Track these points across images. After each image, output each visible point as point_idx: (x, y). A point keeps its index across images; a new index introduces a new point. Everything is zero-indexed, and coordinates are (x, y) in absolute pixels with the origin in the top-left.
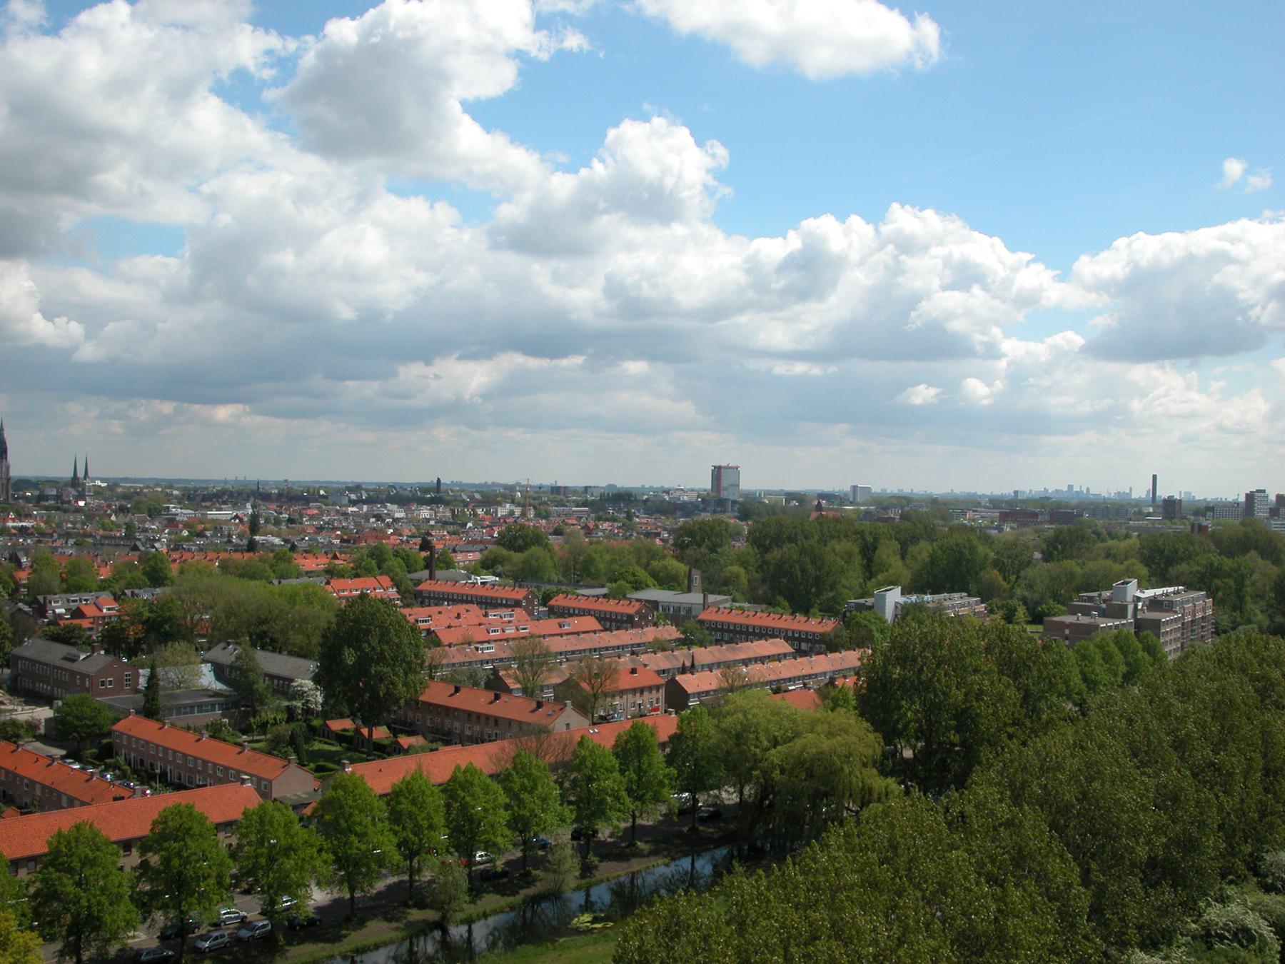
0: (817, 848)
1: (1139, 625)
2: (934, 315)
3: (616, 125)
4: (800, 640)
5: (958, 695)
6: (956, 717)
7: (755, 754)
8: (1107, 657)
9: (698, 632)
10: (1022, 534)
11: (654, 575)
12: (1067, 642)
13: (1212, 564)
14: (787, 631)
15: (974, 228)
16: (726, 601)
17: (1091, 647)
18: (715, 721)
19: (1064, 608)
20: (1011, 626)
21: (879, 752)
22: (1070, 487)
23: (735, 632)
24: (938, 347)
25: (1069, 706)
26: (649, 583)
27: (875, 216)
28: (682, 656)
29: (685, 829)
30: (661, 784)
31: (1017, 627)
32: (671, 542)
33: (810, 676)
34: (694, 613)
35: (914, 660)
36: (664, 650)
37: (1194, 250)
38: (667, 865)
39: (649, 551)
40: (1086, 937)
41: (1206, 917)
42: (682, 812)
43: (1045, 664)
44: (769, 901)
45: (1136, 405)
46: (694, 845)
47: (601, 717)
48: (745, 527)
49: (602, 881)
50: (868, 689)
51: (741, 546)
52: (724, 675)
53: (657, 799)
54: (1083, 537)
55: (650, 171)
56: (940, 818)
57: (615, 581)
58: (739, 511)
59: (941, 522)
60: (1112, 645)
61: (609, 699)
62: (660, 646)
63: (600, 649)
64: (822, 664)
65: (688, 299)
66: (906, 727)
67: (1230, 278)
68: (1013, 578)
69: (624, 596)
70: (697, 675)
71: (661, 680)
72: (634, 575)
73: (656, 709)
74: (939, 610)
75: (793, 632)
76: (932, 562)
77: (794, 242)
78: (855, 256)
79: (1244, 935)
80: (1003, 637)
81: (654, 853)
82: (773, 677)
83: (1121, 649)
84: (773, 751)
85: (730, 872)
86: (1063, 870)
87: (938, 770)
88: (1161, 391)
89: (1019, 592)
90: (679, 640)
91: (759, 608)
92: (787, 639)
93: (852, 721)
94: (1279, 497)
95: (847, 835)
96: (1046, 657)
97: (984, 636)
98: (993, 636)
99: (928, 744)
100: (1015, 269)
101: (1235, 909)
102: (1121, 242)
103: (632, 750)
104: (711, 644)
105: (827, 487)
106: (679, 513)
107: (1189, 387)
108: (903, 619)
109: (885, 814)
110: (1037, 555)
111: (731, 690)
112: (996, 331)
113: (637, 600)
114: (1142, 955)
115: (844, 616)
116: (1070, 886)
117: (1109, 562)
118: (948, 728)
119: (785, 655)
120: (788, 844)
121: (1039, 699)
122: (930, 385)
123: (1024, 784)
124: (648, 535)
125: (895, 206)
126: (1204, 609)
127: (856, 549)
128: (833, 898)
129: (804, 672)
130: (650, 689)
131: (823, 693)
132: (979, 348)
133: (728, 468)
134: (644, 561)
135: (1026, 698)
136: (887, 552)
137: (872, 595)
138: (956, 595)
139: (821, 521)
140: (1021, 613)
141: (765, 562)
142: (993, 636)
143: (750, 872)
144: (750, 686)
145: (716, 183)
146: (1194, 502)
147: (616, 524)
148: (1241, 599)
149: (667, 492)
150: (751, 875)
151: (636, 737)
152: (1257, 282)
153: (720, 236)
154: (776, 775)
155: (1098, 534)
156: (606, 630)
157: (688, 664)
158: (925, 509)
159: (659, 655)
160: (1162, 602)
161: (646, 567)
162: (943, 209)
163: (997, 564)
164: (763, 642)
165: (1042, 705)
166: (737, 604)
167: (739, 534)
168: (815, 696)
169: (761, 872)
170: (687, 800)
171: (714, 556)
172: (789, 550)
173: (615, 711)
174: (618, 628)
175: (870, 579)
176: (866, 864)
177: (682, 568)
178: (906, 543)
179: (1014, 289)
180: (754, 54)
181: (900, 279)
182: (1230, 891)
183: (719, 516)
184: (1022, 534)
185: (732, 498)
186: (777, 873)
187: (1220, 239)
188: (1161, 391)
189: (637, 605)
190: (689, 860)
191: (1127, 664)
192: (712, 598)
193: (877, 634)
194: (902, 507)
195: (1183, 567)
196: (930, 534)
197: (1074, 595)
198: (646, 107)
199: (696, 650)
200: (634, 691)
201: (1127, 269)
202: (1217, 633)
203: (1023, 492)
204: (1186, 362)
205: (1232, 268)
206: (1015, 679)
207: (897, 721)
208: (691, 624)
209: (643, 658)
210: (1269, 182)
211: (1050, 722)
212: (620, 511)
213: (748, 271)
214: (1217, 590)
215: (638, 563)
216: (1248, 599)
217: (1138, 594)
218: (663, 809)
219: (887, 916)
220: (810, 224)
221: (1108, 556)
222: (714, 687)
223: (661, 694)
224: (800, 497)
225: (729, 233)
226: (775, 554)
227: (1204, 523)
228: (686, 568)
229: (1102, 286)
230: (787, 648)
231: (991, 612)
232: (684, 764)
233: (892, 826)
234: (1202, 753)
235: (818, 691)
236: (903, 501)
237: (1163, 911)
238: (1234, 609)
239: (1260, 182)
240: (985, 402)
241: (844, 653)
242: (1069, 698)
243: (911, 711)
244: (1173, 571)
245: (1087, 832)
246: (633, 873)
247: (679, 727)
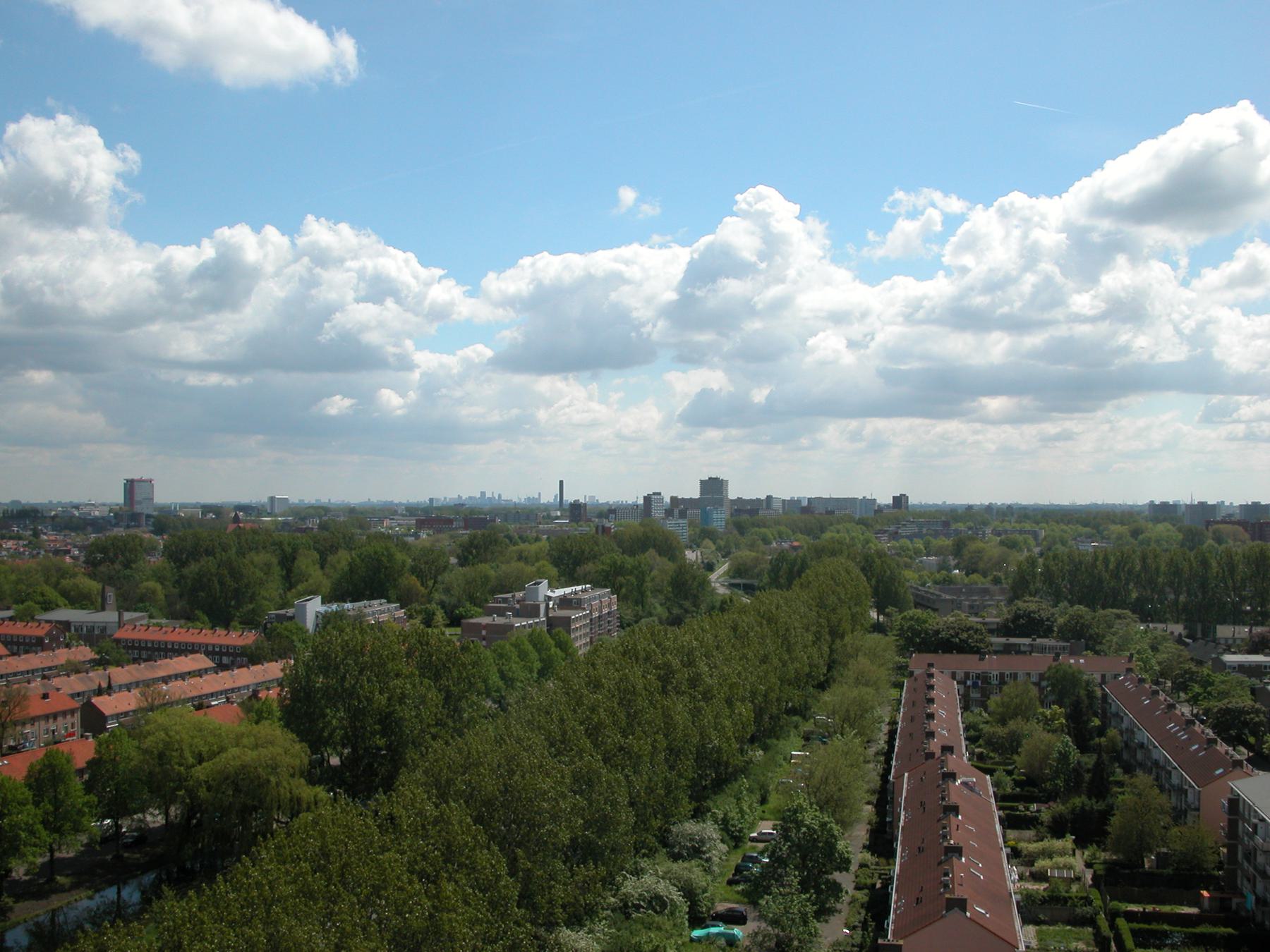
0: (249, 864)
1: (551, 623)
2: (349, 326)
3: (17, 119)
4: (221, 654)
5: (381, 699)
6: (380, 722)
7: (179, 773)
8: (523, 655)
9: (112, 653)
10: (438, 541)
11: (65, 594)
12: (484, 643)
13: (615, 563)
14: (207, 645)
15: (389, 243)
16: (141, 618)
17: (508, 646)
18: (136, 743)
19: (480, 610)
20: (430, 630)
21: (306, 761)
22: (483, 494)
23: (153, 649)
24: (353, 358)
25: (489, 703)
26: (60, 603)
27: (291, 228)
28: (97, 677)
29: (109, 857)
30: (80, 813)
31: (435, 631)
32: (82, 559)
33: (233, 690)
34: (109, 632)
35: (337, 668)
36: (78, 672)
37: (592, 271)
38: (91, 898)
39: (59, 569)
40: (517, 924)
41: (623, 890)
42: (105, 840)
43: (463, 665)
44: (203, 923)
45: (542, 415)
46: (118, 873)
47: (11, 748)
48: (161, 541)
49: (19, 923)
50: (292, 699)
51: (156, 560)
52: (143, 694)
53: (77, 829)
54: (496, 541)
55: (54, 170)
56: (370, 821)
57: (22, 602)
58: (154, 525)
59: (359, 531)
60: (526, 643)
61: (19, 728)
62: (73, 669)
63: (7, 675)
64: (244, 677)
65: (95, 307)
66: (331, 735)
67: (623, 296)
68: (430, 583)
69: (33, 618)
70: (114, 696)
71: (76, 704)
72: (43, 595)
73: (72, 735)
74: (360, 617)
75: (214, 646)
76: (351, 570)
77: (208, 251)
78: (270, 268)
79: (658, 903)
80: (423, 641)
81: (75, 886)
82: (195, 693)
83: (535, 646)
84: (199, 768)
85: (159, 898)
86: (490, 860)
87: (365, 776)
88: (565, 401)
89: (437, 596)
90: (93, 661)
91: (177, 623)
92: (207, 654)
93: (278, 732)
94: (674, 499)
95: (278, 847)
96: (466, 658)
97: (404, 641)
98: (413, 641)
99: (354, 749)
100: (428, 284)
101: (648, 879)
102: (526, 261)
103: (46, 780)
104: (128, 663)
105: (244, 499)
106: (90, 529)
107: (590, 398)
108: (324, 628)
109: (315, 823)
110: (453, 560)
111: (152, 709)
112: (409, 344)
113: (47, 621)
114: (569, 932)
115: (265, 628)
116: (498, 878)
117: (521, 564)
118: (373, 734)
119: (206, 670)
120: (219, 862)
121: (460, 700)
122: (346, 395)
123: (449, 782)
124: (57, 552)
125: (310, 218)
126: (610, 605)
127: (275, 560)
128: (268, 912)
129: (227, 686)
130: (64, 714)
131: (246, 707)
132: (391, 360)
133: (141, 481)
134: (54, 580)
135: (448, 698)
136: (306, 562)
137: (293, 606)
138: (376, 602)
139: (239, 533)
140: (440, 616)
141: (182, 577)
142: (413, 641)
143: (182, 895)
144: (171, 704)
145: (126, 190)
146: (598, 505)
147: (21, 543)
148: (642, 594)
149: (77, 507)
150: (182, 898)
151: (51, 766)
152: (649, 300)
153: (130, 243)
154: (203, 793)
155: (510, 538)
156: (13, 654)
157: (104, 685)
158: (342, 519)
159: (73, 677)
160: (571, 600)
161: (56, 586)
162: (358, 224)
163: (414, 570)
164: (183, 658)
165: (463, 704)
166: (154, 621)
167: (155, 549)
168: (239, 710)
169: (191, 893)
170: (109, 827)
171: (128, 572)
172: (208, 563)
173: (26, 739)
174: (27, 652)
175: (290, 589)
176: (298, 875)
177: (94, 586)
178: (325, 552)
179: (427, 303)
180: (167, 55)
181: (313, 292)
182: (644, 863)
183: (133, 531)
184: (438, 541)
185: (146, 512)
186: (208, 892)
187: (616, 260)
188: (565, 401)
189: (47, 627)
190: (114, 889)
191: (541, 660)
192: (127, 616)
193: (299, 645)
194: (320, 518)
195: (590, 567)
196: (349, 543)
197: (489, 597)
198: (50, 102)
199: (113, 670)
200: (47, 717)
201: (531, 287)
202: (622, 627)
203: (438, 500)
204: (588, 374)
205: (626, 288)
206: (436, 681)
207: (322, 730)
208: (106, 644)
209: (55, 682)
210: (658, 210)
211: (471, 719)
212: (25, 528)
213: (160, 280)
214: (621, 586)
215: (46, 582)
216: (649, 593)
217: (549, 593)
218: (84, 838)
219: (323, 924)
220: (225, 233)
221: (520, 558)
222: (132, 707)
223: (77, 718)
224: (217, 510)
225: (140, 239)
226: (193, 568)
227: (608, 525)
228: (100, 586)
229: (509, 302)
230: (209, 663)
231: (410, 617)
232: (104, 789)
233: (323, 834)
234: (613, 738)
235: (241, 704)
236: (321, 510)
237: (585, 888)
238: (637, 603)
239: (649, 210)
240: (399, 412)
241: (266, 665)
242: (488, 696)
243: (336, 718)
244: (580, 570)
245: (507, 819)
246: (54, 911)
247: (98, 752)
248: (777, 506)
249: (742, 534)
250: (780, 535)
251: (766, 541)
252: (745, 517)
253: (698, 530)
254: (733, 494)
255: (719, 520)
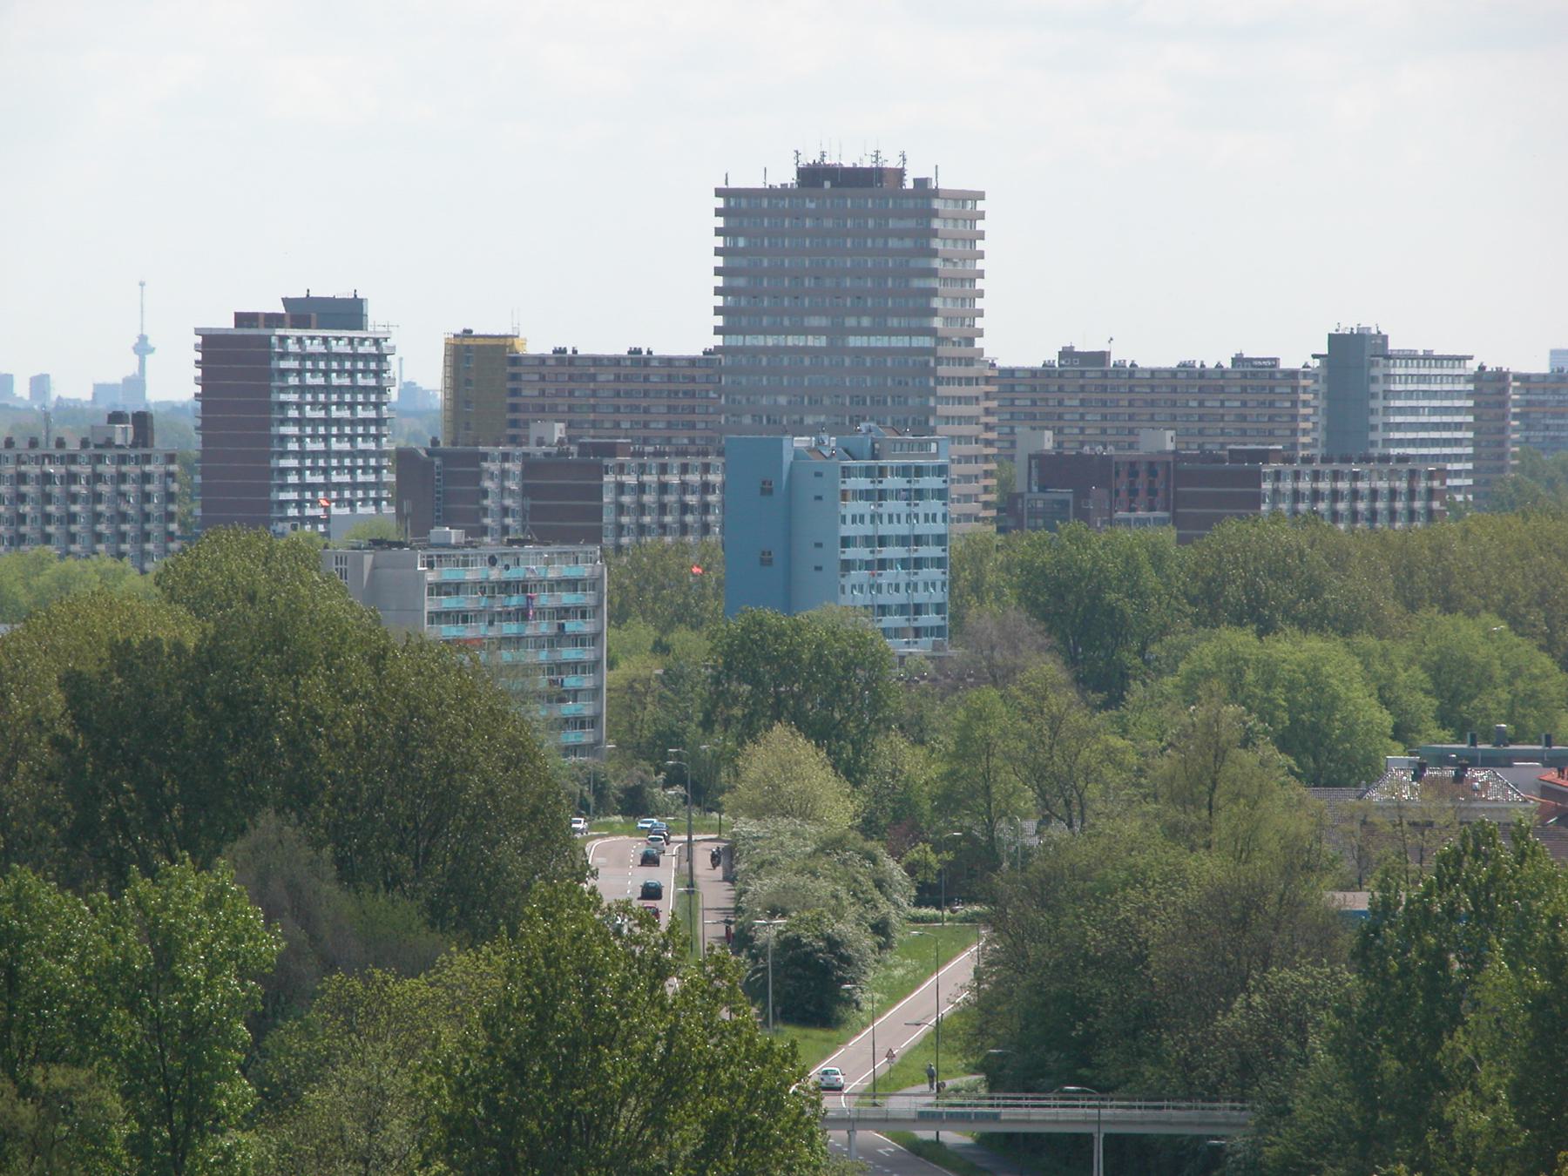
94: (480, 363)
248: (1415, 425)
249: (1105, 684)
250: (1454, 688)
251: (1323, 752)
252: (1138, 535)
253: (691, 644)
254: (1021, 319)
255: (895, 558)
